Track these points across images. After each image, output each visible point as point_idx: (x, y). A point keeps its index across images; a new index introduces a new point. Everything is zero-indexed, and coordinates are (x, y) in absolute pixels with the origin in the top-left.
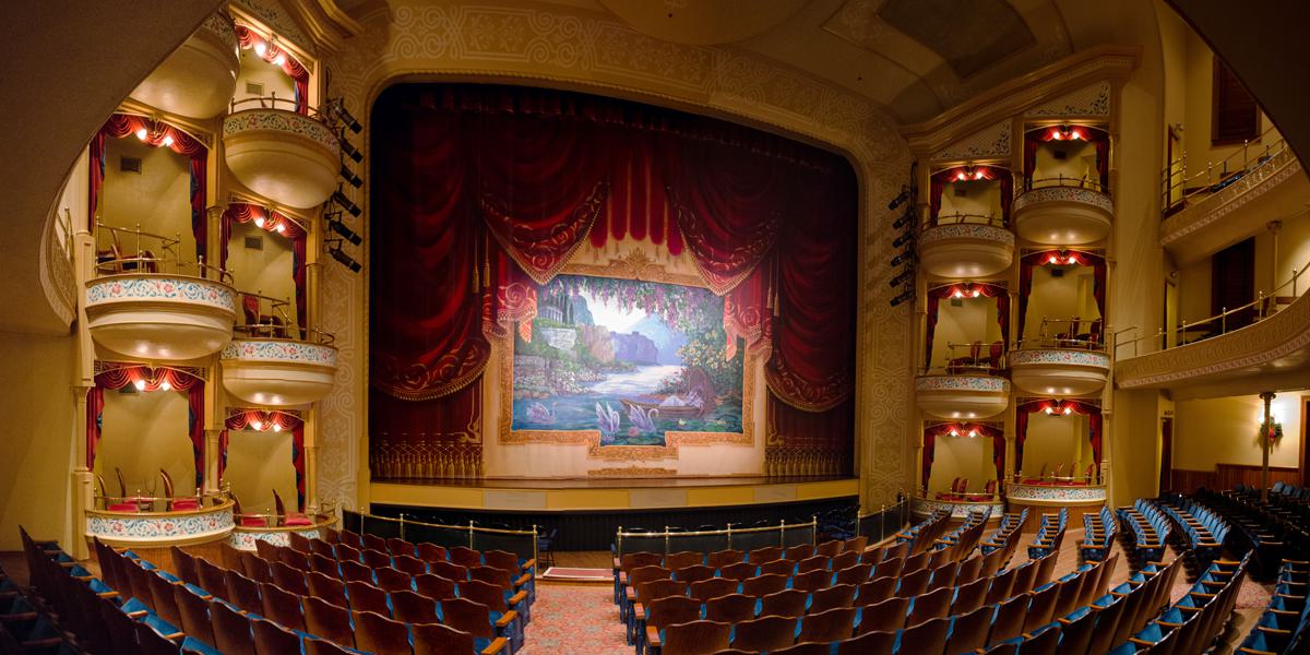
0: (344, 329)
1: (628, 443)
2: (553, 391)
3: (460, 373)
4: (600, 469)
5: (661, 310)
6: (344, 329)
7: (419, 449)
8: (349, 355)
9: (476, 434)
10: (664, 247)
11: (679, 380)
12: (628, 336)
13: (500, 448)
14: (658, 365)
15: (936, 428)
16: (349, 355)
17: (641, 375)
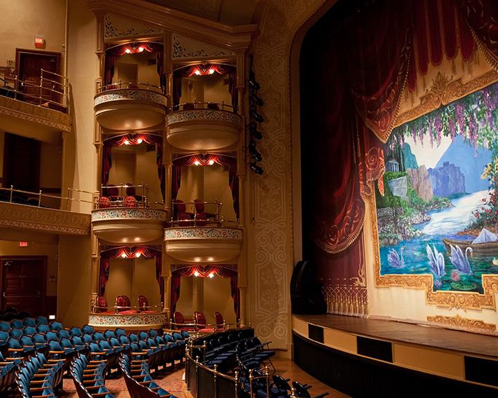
0: (279, 209)
1: (452, 289)
2: (400, 237)
3: (352, 228)
4: (435, 316)
5: (463, 129)
6: (279, 209)
7: (336, 291)
8: (283, 225)
9: (363, 278)
10: (459, 58)
11: (488, 208)
12: (440, 169)
13: (376, 290)
14: (468, 194)
15: (181, 270)
16: (283, 225)
17: (453, 210)
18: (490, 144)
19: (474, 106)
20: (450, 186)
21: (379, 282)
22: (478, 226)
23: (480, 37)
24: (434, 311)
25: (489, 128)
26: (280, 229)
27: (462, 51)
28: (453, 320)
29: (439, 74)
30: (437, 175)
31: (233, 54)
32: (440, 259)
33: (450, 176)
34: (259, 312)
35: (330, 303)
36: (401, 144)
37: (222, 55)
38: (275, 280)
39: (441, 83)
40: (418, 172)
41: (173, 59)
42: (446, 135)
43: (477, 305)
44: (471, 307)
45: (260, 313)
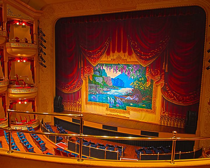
1: (116, 108)
3: (77, 87)
5: (125, 72)
7: (68, 104)
13: (85, 105)
18: (133, 78)
19: (130, 68)
20: (118, 83)
21: (86, 103)
22: (127, 95)
23: (135, 52)
24: (109, 113)
25: (134, 74)
26: (48, 85)
27: (128, 53)
28: (116, 115)
29: (119, 55)
30: (115, 81)
31: (33, 19)
32: (112, 101)
33: (119, 82)
34: (203, 134)
35: (65, 108)
36: (101, 68)
37: (29, 19)
38: (46, 101)
39: (119, 58)
40: (107, 78)
41: (7, 15)
42: (119, 71)
43: (124, 113)
44: (122, 113)
45: (203, 135)
